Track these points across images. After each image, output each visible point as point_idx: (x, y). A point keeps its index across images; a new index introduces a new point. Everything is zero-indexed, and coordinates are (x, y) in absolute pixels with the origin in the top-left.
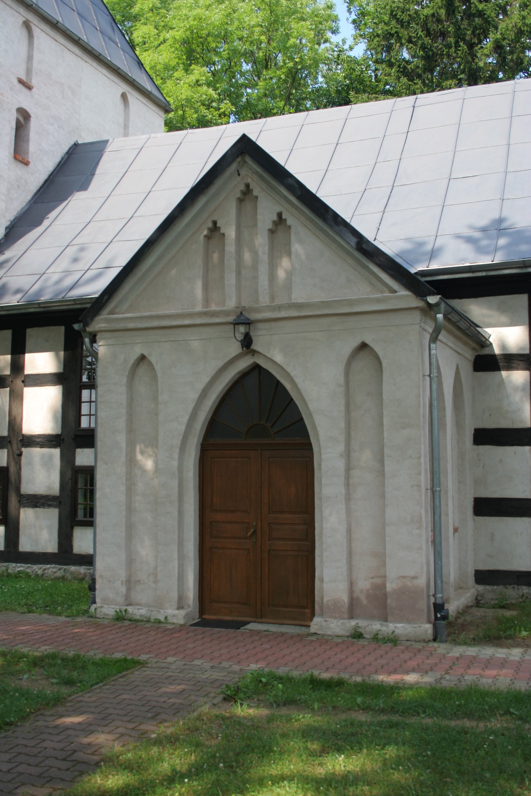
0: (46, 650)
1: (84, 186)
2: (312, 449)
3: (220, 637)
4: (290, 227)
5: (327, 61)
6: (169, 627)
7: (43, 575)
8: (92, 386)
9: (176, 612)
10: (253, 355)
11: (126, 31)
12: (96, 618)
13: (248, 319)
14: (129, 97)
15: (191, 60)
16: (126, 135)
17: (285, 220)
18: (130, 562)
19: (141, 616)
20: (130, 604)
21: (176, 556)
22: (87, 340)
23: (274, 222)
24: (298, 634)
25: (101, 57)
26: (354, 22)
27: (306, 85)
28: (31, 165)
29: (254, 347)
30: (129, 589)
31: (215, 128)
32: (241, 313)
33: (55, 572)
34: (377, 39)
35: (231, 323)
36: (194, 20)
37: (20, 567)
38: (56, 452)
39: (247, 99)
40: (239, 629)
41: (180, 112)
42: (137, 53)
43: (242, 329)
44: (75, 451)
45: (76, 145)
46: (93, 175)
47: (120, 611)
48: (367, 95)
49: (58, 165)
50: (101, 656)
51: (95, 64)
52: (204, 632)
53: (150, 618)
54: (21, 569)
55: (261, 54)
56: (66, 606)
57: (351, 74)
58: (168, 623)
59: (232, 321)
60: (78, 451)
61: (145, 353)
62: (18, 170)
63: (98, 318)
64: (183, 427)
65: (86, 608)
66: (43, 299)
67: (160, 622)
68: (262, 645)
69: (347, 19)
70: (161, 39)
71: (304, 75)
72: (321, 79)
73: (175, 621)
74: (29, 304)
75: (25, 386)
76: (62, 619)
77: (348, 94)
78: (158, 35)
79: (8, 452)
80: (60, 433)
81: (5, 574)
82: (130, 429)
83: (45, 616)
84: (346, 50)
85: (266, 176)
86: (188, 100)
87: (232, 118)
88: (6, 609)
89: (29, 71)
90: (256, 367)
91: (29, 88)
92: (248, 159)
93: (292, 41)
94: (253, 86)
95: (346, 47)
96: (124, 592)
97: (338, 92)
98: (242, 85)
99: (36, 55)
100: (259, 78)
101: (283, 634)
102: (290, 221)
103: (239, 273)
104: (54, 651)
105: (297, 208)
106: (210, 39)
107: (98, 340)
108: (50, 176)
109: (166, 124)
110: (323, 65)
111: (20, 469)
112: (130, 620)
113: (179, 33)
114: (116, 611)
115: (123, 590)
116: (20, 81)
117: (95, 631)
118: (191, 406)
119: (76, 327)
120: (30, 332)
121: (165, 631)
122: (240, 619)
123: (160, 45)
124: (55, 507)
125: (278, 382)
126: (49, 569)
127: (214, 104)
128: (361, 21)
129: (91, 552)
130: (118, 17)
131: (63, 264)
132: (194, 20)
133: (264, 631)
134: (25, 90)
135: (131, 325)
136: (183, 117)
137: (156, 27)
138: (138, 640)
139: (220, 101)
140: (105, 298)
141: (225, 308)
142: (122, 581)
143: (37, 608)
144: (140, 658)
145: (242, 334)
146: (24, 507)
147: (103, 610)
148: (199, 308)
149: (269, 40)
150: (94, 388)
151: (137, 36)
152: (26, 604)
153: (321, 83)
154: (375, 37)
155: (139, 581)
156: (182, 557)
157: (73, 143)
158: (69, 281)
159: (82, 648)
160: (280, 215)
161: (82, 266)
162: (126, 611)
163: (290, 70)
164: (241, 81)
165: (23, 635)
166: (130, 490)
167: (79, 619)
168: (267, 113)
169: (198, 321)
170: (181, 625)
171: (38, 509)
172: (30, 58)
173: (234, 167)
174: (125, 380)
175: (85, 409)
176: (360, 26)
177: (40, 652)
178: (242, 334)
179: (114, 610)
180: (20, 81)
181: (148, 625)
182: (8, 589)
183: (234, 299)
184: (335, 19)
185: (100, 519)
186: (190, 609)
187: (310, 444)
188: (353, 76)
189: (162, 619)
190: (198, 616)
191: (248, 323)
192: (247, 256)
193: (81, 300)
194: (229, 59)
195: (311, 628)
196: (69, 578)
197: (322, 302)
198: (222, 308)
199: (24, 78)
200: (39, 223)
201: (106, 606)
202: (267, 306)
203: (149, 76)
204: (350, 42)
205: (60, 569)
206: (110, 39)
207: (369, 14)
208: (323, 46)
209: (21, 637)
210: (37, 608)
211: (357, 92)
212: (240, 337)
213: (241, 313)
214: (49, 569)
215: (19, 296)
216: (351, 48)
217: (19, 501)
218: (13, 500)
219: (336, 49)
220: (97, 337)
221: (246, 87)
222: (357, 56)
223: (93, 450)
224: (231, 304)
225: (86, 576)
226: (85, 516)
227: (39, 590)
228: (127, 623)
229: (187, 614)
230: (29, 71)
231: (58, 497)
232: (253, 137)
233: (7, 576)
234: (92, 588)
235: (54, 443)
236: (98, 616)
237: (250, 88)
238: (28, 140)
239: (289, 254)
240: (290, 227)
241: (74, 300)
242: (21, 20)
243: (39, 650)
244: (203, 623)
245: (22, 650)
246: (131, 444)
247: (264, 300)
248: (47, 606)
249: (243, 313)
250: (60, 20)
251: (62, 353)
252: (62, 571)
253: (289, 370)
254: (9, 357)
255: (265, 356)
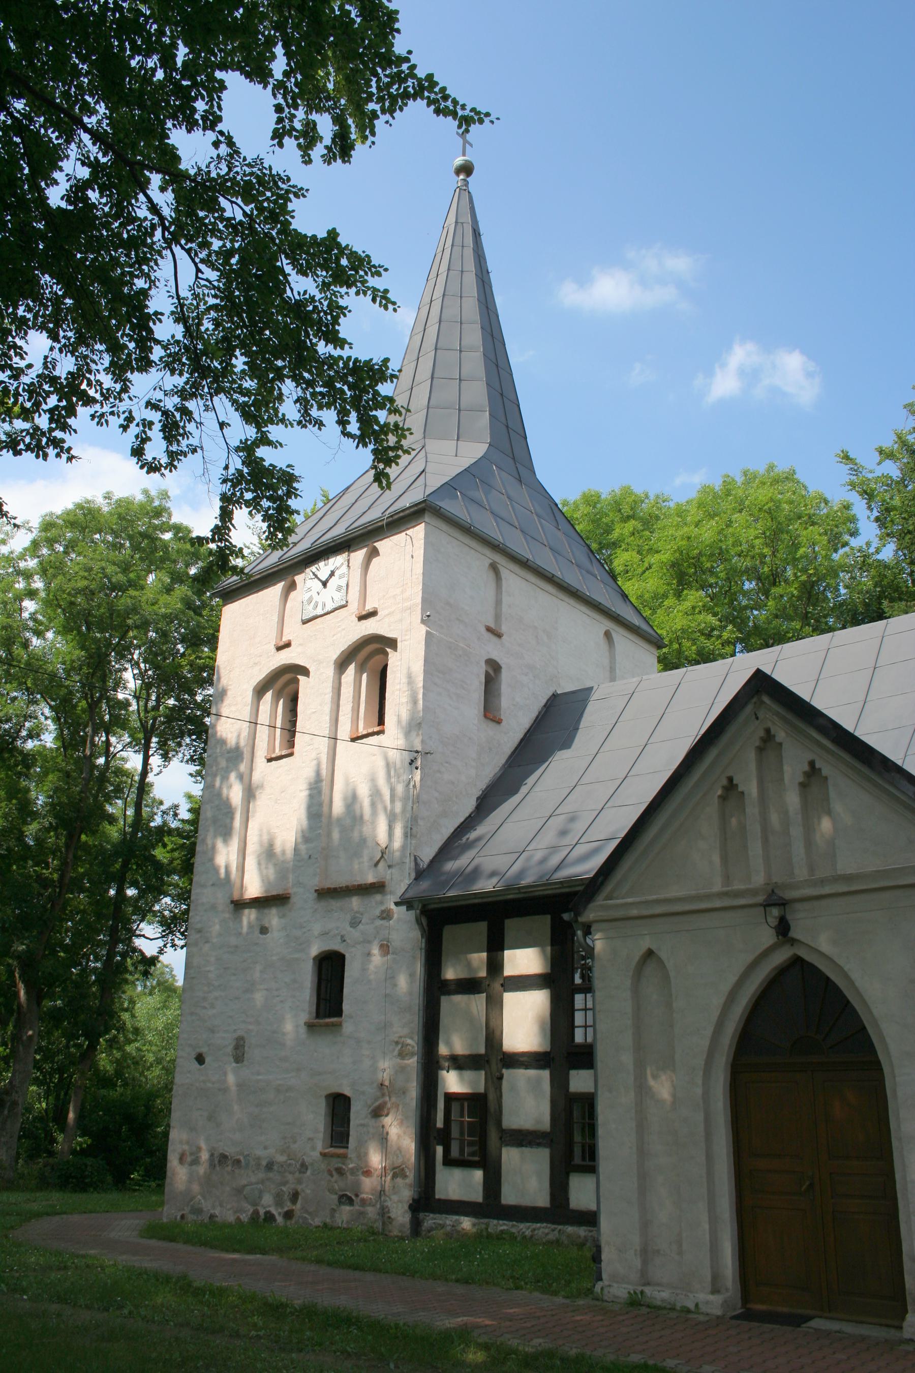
0: (540, 1344)
1: (567, 744)
2: (882, 1069)
3: (773, 1338)
4: (826, 778)
5: (844, 567)
6: (702, 1318)
7: (532, 1237)
8: (587, 988)
9: (711, 1297)
10: (792, 945)
11: (604, 560)
12: (603, 1301)
13: (782, 898)
14: (614, 635)
15: (683, 585)
16: (613, 679)
17: (820, 770)
18: (645, 1225)
19: (663, 1300)
20: (648, 1284)
21: (704, 1218)
22: (579, 933)
23: (805, 773)
24: (886, 1341)
25: (579, 593)
26: (877, 519)
27: (826, 599)
28: (504, 723)
29: (793, 934)
30: (645, 1262)
31: (720, 662)
32: (773, 891)
33: (547, 1234)
34: (909, 536)
35: (761, 905)
36: (682, 539)
37: (502, 1225)
38: (546, 1074)
39: (754, 623)
40: (799, 1326)
41: (676, 646)
42: (619, 583)
43: (775, 912)
44: (568, 1074)
45: (555, 696)
46: (577, 729)
47: (635, 1293)
48: (904, 603)
49: (535, 721)
50: (611, 1358)
51: (572, 602)
52: (750, 1329)
53: (675, 1305)
54: (505, 1227)
55: (766, 569)
56: (563, 1282)
57: (881, 581)
58: (699, 1314)
59: (761, 901)
60: (573, 1073)
61: (654, 948)
62: (489, 730)
63: (591, 906)
64: (705, 1043)
65: (589, 1285)
66: (524, 882)
67: (689, 1311)
68: (834, 1353)
69: (868, 517)
70: (646, 564)
71: (822, 588)
72: (843, 591)
73: (709, 1311)
74: (508, 889)
75: (505, 991)
76: (559, 1300)
77: (880, 604)
78: (642, 560)
79: (486, 1074)
80: (549, 1050)
81: (485, 1234)
82: (639, 1048)
83: (536, 1294)
84: (873, 554)
85: (790, 716)
86: (683, 631)
87: (739, 647)
88: (487, 1283)
89: (498, 617)
90: (797, 961)
91: (499, 636)
92: (766, 699)
93: (801, 551)
94: (758, 607)
95: (872, 550)
96: (639, 1267)
97: (867, 605)
98: (746, 607)
99: (505, 599)
100: (767, 598)
101: (863, 1338)
102: (826, 771)
103: (765, 841)
104: (551, 1346)
105: (828, 750)
106: (704, 559)
107: (593, 932)
108: (526, 735)
109: (660, 660)
110: (844, 573)
111: (501, 1096)
112: (648, 1306)
113: (666, 556)
114: (629, 1293)
115: (638, 1263)
116: (489, 629)
117: (602, 1320)
118: (716, 1013)
119: (566, 916)
120: (508, 923)
121: (696, 1325)
122: (800, 1311)
123: (644, 572)
124: (545, 1146)
125: (828, 978)
126: (539, 1229)
127: (716, 633)
128: (886, 518)
129: (593, 1207)
130: (594, 546)
131: (548, 838)
132: (682, 539)
133: (836, 1332)
134: (494, 639)
135: (634, 912)
136: (679, 652)
137: (639, 552)
138: (661, 1337)
139: (724, 628)
140: (600, 879)
141: (751, 886)
142: (636, 1250)
143: (526, 1284)
144: (665, 1364)
145: (776, 918)
146: (507, 1145)
147: (611, 1290)
148: (717, 887)
149: (774, 552)
150: (590, 992)
151: (618, 565)
152: (512, 1277)
153: (844, 595)
154: (906, 534)
155: (658, 1251)
156: (713, 1219)
157: (551, 694)
158: (555, 860)
159: (587, 1345)
160: (812, 764)
161: (570, 840)
162: (642, 1292)
163: (803, 584)
164: (745, 602)
165: (510, 1320)
166: (641, 1127)
167: (581, 1302)
168: (780, 638)
169: (717, 904)
170: (718, 1317)
171: (524, 1148)
172: (498, 602)
173: (749, 708)
174: (628, 983)
175: (579, 1018)
176: (885, 523)
177: (532, 1347)
178: (776, 918)
179: (626, 1291)
180: (489, 629)
181: (673, 1315)
182: (489, 1254)
183: (762, 874)
184: (853, 520)
185: (604, 1165)
186: (729, 1294)
187: (878, 1063)
188: (885, 582)
189: (691, 1306)
190: (740, 1305)
191: (783, 904)
192: (774, 819)
193: (569, 882)
194: (728, 579)
195: (905, 1330)
196: (566, 1242)
197: (878, 871)
198: (748, 886)
199: (492, 626)
200: (515, 791)
201: (615, 1285)
202: (806, 881)
203: (636, 608)
204: (875, 543)
205: (553, 1230)
206: (588, 572)
207: (895, 508)
208: (841, 551)
209: (508, 1323)
210: (526, 1284)
211: (892, 600)
212: (773, 922)
213: (773, 891)
214: (539, 1229)
215: (494, 880)
216: (878, 551)
217: (501, 1138)
218: (493, 1136)
219: (859, 554)
220: (592, 929)
221: (752, 609)
222: (886, 560)
223: (592, 1071)
224: (759, 879)
225: (587, 1241)
226: (584, 1159)
227: (527, 1257)
228: (644, 1310)
229: (725, 1301)
230: (498, 617)
231: (549, 1133)
232: (768, 671)
233: (487, 1238)
234: (597, 1258)
235: (542, 1062)
236: (606, 1298)
237: (756, 610)
238: (499, 695)
239: (829, 812)
240: (826, 778)
241: (561, 882)
242: (487, 562)
243: (531, 1343)
244: (748, 1316)
245: (510, 1343)
246: (640, 1067)
247: (801, 873)
248: (538, 1281)
249: (776, 891)
250: (530, 557)
251: (549, 949)
252: (556, 1232)
253: (841, 962)
254: (485, 954)
255: (807, 945)
